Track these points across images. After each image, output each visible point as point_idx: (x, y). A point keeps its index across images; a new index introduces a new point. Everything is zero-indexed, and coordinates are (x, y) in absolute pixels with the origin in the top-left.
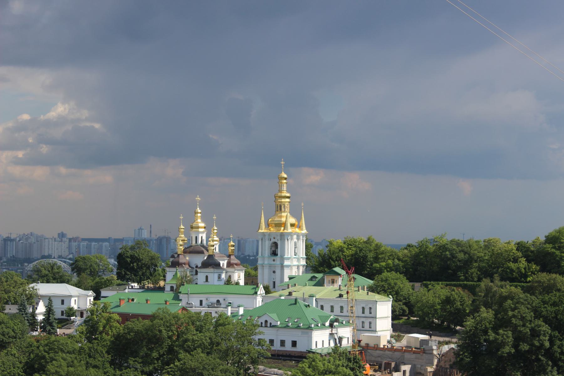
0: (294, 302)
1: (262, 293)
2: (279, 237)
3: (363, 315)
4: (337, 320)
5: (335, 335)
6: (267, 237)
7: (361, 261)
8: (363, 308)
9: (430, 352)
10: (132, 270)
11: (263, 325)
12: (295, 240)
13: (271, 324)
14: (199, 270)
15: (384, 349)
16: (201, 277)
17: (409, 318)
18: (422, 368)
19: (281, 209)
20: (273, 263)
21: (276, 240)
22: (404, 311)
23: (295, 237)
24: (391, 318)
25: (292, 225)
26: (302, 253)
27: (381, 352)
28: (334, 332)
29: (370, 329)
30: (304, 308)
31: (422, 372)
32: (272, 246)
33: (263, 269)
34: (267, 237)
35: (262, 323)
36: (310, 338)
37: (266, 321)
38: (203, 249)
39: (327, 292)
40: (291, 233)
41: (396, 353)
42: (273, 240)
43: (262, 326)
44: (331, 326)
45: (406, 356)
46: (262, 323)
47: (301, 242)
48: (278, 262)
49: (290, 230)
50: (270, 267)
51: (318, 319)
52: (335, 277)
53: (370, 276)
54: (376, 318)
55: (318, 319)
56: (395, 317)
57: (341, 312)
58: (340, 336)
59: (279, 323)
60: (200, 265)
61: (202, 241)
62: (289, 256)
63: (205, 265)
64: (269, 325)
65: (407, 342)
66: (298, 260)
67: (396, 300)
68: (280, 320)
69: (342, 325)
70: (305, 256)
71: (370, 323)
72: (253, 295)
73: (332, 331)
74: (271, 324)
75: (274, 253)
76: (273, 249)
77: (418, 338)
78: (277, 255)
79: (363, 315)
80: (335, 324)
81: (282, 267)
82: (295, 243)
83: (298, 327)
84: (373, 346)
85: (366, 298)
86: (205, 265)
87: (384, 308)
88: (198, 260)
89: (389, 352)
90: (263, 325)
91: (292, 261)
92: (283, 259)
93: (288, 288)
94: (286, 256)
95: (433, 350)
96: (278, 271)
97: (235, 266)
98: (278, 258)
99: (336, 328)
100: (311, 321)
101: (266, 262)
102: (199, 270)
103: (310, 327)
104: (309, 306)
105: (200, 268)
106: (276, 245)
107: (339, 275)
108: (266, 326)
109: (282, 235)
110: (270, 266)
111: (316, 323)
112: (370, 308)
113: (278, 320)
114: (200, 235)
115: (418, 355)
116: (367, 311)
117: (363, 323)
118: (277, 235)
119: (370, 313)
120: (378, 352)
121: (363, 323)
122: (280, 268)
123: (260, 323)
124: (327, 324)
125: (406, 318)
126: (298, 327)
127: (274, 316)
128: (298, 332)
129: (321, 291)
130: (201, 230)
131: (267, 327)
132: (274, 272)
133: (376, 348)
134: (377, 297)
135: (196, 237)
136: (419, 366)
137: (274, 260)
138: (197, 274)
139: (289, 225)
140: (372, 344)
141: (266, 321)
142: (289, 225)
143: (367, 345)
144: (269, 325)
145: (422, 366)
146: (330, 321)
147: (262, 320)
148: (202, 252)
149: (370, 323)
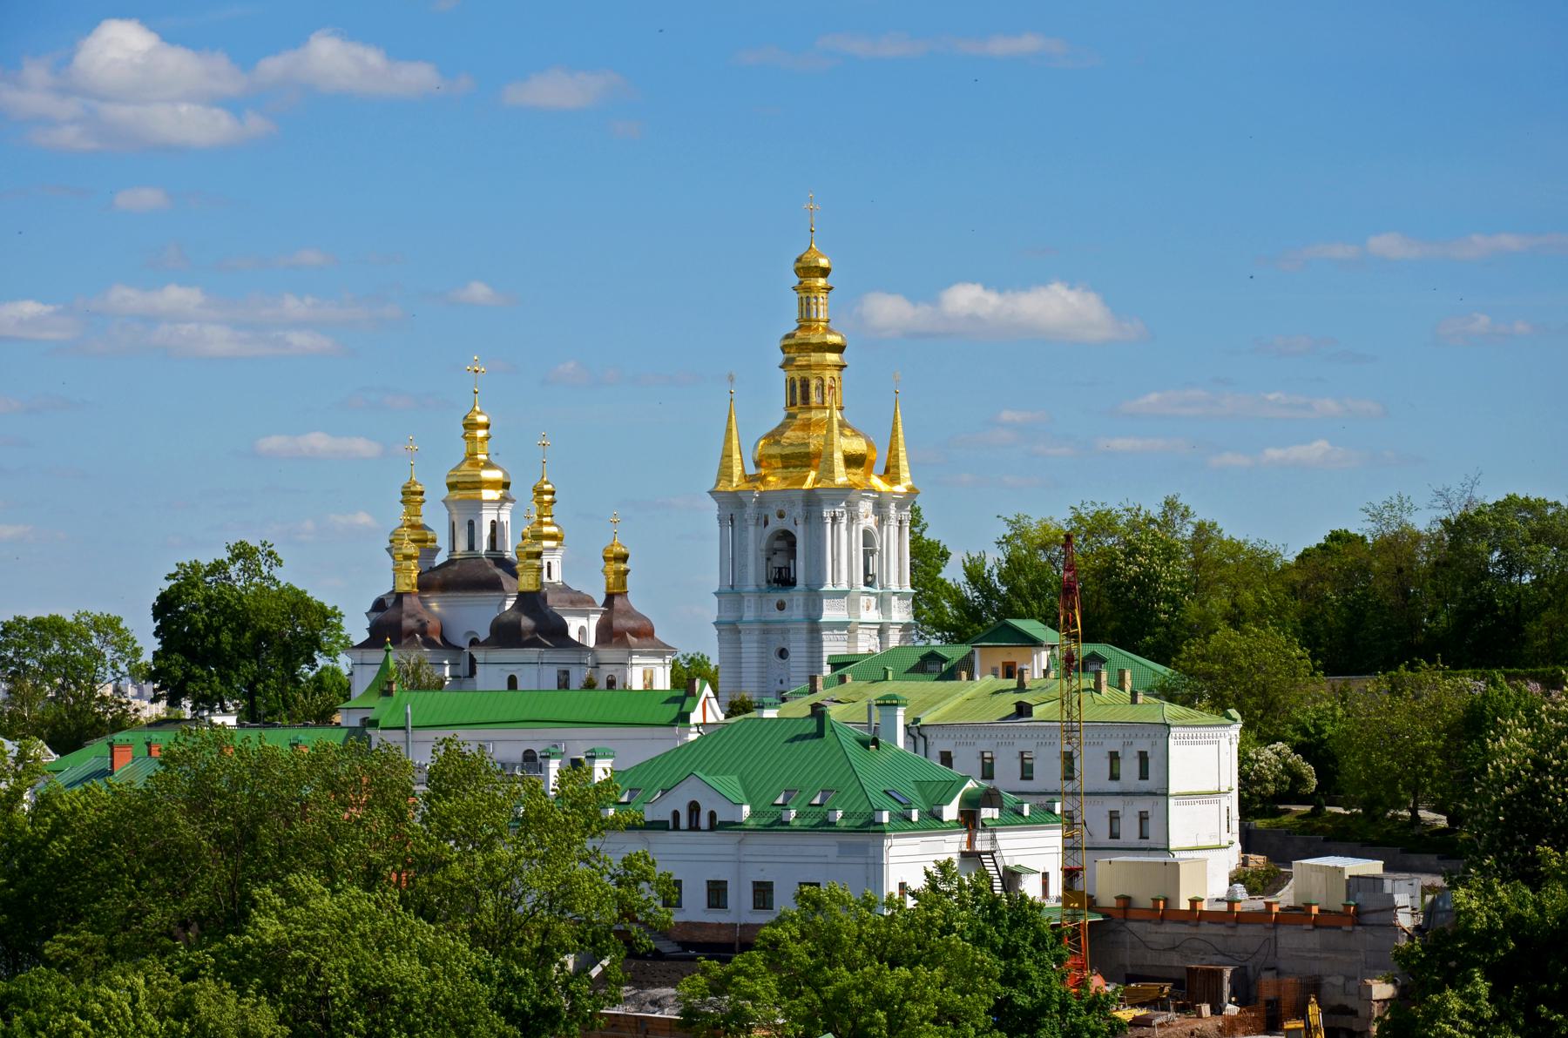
0: (812, 726)
1: (710, 719)
2: (798, 511)
3: (1114, 786)
4: (990, 798)
5: (987, 860)
6: (750, 511)
7: (1124, 600)
8: (1114, 757)
9: (1383, 917)
10: (213, 656)
11: (684, 822)
12: (870, 522)
13: (712, 815)
14: (479, 655)
15: (1195, 916)
16: (490, 676)
17: (1317, 812)
18: (1352, 986)
19: (806, 397)
20: (776, 615)
21: (786, 524)
22: (1298, 779)
23: (866, 507)
24: (1232, 802)
25: (853, 461)
26: (897, 573)
27: (1183, 929)
28: (979, 847)
29: (1144, 843)
30: (853, 750)
31: (1352, 1003)
32: (772, 552)
33: (739, 641)
34: (750, 511)
35: (676, 815)
36: (875, 869)
37: (694, 808)
38: (499, 571)
39: (973, 697)
40: (848, 489)
41: (1243, 930)
42: (775, 524)
43: (676, 828)
44: (969, 819)
45: (1282, 942)
46: (676, 815)
47: (894, 531)
48: (796, 611)
49: (841, 476)
50: (765, 632)
51: (912, 793)
52: (1015, 655)
53: (1161, 654)
54: (1166, 795)
55: (912, 793)
56: (1257, 801)
57: (1023, 778)
58: (1010, 863)
59: (746, 809)
60: (484, 634)
61: (493, 539)
62: (844, 586)
63: (505, 635)
64: (704, 822)
65: (1296, 895)
66: (883, 603)
67: (1258, 731)
68: (750, 801)
69: (1014, 818)
70: (908, 589)
71: (1143, 817)
72: (672, 724)
73: (971, 842)
74: (712, 815)
75: (784, 580)
76: (779, 561)
77: (1341, 870)
78: (794, 584)
79: (1069, 786)
80: (987, 813)
81: (815, 629)
82: (867, 533)
83: (826, 825)
84: (1150, 905)
85: (1129, 714)
86: (505, 635)
87: (1205, 762)
88: (474, 615)
89: (1214, 929)
90: (684, 822)
91: (854, 606)
92: (815, 596)
93: (813, 690)
94: (828, 587)
95: (1395, 908)
96: (798, 649)
97: (632, 639)
98: (796, 598)
99: (992, 828)
100: (877, 798)
101: (749, 614)
102: (479, 655)
103: (872, 822)
104: (875, 742)
105: (486, 643)
106: (788, 539)
107: (1034, 643)
108: (694, 827)
109: (812, 502)
110: (766, 629)
111: (899, 809)
112: (1143, 757)
113: (744, 799)
114: (488, 516)
115: (1333, 936)
116: (1129, 767)
117: (1114, 817)
118: (792, 503)
119: (1144, 775)
120: (1168, 928)
121: (1114, 817)
122: (804, 635)
123: (668, 817)
124: (951, 812)
125: (1308, 808)
126: (826, 825)
127: (730, 785)
128: (825, 846)
129: (947, 696)
130: (488, 494)
131: (697, 829)
132: (783, 653)
133: (1164, 912)
134: (1171, 710)
135: (471, 524)
136: (1340, 981)
137: (781, 606)
138: (472, 673)
139: (838, 457)
140: (1143, 900)
141: (694, 808)
142: (838, 457)
143: (1125, 901)
144: (704, 822)
145: (1348, 978)
146: (964, 801)
147: (679, 802)
148: (494, 585)
149: (1143, 817)
